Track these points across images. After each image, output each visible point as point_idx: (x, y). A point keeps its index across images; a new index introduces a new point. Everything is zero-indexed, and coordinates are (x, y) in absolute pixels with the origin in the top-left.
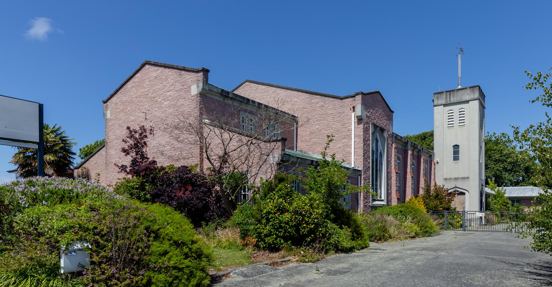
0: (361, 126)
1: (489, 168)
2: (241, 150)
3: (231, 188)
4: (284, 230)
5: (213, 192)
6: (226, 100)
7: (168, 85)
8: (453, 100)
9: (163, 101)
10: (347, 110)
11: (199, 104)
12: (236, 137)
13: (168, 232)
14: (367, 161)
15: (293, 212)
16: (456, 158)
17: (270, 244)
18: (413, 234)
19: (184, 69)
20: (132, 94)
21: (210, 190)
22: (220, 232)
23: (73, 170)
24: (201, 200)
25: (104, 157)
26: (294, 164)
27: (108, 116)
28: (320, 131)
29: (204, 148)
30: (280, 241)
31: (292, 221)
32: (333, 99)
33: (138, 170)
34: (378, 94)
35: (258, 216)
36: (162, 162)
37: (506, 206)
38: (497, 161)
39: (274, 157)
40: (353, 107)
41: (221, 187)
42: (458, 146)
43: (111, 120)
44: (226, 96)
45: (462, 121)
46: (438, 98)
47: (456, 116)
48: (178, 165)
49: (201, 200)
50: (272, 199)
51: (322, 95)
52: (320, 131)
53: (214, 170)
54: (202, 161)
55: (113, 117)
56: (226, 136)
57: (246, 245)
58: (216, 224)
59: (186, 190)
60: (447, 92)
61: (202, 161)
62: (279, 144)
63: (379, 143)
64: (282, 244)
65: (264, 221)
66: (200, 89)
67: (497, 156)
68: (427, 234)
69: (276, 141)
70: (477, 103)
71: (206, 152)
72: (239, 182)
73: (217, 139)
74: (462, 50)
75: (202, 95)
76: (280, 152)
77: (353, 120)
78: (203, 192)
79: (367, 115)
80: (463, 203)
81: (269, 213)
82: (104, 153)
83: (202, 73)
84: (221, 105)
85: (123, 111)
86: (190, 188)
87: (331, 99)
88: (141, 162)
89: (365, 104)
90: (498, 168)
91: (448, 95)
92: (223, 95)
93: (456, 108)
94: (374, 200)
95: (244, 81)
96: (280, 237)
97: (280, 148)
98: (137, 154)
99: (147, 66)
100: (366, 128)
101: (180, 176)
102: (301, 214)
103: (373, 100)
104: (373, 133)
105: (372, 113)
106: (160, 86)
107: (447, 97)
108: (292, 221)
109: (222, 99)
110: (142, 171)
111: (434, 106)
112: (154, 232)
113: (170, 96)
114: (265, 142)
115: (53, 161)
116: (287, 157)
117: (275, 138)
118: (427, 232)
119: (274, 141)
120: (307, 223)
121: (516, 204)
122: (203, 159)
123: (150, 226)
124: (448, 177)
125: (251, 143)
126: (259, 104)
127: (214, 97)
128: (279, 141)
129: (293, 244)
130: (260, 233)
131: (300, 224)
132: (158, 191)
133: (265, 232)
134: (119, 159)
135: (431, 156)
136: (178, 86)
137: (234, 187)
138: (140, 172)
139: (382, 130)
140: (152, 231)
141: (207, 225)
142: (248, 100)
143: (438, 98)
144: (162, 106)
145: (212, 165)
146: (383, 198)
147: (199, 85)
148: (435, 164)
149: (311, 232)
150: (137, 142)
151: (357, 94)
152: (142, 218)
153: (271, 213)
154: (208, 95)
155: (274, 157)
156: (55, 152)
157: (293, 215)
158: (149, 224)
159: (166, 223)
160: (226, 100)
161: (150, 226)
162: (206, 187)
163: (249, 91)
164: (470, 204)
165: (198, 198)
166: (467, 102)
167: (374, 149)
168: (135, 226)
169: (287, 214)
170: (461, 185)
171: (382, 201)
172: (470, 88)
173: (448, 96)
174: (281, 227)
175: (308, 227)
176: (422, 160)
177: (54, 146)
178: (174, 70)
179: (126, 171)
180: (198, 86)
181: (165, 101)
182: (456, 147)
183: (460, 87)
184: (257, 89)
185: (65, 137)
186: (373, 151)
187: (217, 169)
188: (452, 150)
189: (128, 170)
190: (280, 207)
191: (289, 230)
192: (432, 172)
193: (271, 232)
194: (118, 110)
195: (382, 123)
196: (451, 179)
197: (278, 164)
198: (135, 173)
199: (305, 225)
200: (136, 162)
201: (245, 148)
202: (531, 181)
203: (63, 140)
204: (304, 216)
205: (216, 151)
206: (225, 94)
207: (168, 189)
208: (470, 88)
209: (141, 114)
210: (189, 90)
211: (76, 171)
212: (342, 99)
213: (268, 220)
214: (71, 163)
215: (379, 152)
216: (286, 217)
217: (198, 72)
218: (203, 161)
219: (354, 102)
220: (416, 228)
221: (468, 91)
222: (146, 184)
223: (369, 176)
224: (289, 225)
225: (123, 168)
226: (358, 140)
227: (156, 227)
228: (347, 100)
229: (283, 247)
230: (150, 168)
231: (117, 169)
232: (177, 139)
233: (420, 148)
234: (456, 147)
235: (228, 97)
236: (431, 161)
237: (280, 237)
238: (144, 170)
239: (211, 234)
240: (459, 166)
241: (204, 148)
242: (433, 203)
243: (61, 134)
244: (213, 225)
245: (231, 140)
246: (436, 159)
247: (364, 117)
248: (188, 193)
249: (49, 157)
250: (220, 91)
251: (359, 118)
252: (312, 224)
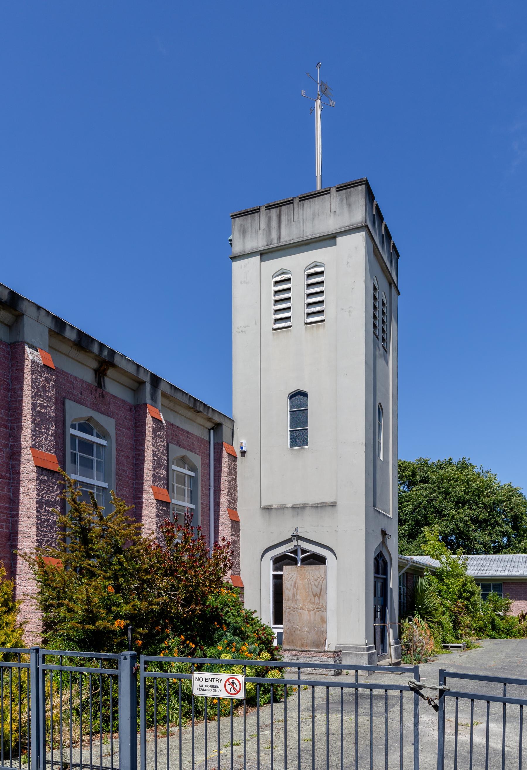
1: (445, 516)
8: (289, 234)
16: (299, 437)
37: (468, 599)
38: (460, 503)
42: (305, 395)
45: (316, 310)
67: (459, 491)
90: (462, 516)
93: (296, 264)
107: (269, 225)
111: (234, 258)
121: (491, 595)
148: (233, 458)
166: (330, 239)
172: (339, 189)
173: (274, 223)
182: (299, 397)
188: (283, 410)
192: (224, 484)
196: (281, 508)
221: (335, 200)
234: (299, 397)
236: (218, 447)
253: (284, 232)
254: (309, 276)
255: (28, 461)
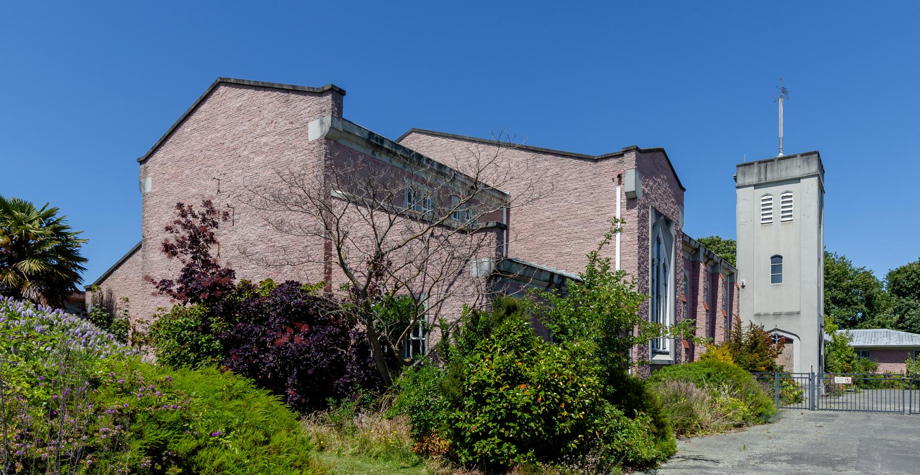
0: (635, 211)
2: (411, 250)
3: (391, 328)
4: (520, 424)
5: (351, 335)
6: (377, 155)
7: (263, 123)
8: (770, 177)
9: (251, 156)
10: (607, 181)
11: (323, 158)
12: (400, 224)
13: (222, 458)
14: (644, 278)
15: (538, 383)
17: (484, 457)
18: (739, 420)
19: (295, 90)
20: (193, 143)
21: (344, 331)
22: (365, 418)
23: (84, 293)
24: (328, 352)
25: (140, 267)
26: (523, 279)
27: (149, 188)
28: (553, 221)
29: (334, 241)
30: (509, 448)
31: (538, 405)
32: (578, 161)
33: (195, 289)
34: (661, 153)
35: (454, 390)
36: (248, 273)
39: (479, 265)
40: (619, 176)
41: (369, 326)
42: (781, 257)
43: (153, 194)
44: (377, 146)
45: (787, 214)
46: (744, 174)
47: (777, 205)
48: (279, 280)
49: (328, 352)
50: (487, 351)
51: (556, 154)
52: (553, 221)
53: (355, 289)
54: (328, 272)
55: (157, 189)
56: (382, 220)
57: (425, 453)
58: (357, 402)
59: (297, 331)
60: (760, 162)
61: (328, 272)
62: (492, 235)
63: (663, 246)
64: (513, 456)
65: (469, 402)
66: (326, 128)
68: (762, 420)
69: (485, 230)
70: (814, 181)
71: (339, 249)
72: (405, 316)
73: (360, 226)
74: (784, 91)
75: (331, 139)
76: (493, 253)
77: (619, 199)
78: (330, 335)
79: (644, 191)
80: (790, 358)
81: (481, 385)
82: (140, 259)
83: (329, 97)
84: (365, 161)
85: (175, 177)
86: (305, 328)
87: (574, 161)
88: (204, 274)
89: (642, 171)
91: (763, 168)
92: (371, 143)
94: (655, 353)
95: (408, 131)
96: (507, 440)
97: (494, 245)
98: (194, 258)
99: (222, 89)
100: (643, 215)
101: (282, 303)
102: (556, 389)
103: (654, 162)
104: (654, 227)
105: (651, 188)
106: (247, 126)
108: (538, 405)
109: (370, 151)
110: (202, 291)
111: (738, 187)
112: (178, 461)
113: (266, 144)
114: (462, 232)
115: (37, 273)
116: (507, 264)
117: (482, 225)
118: (760, 415)
119: (481, 230)
120: (570, 408)
122: (330, 269)
123: (166, 441)
124: (762, 311)
125: (432, 235)
126: (440, 166)
127: (354, 146)
128: (491, 229)
129: (539, 456)
130: (458, 431)
131: (555, 412)
132: (237, 332)
133: (474, 428)
134: (167, 271)
135: (732, 276)
136: (283, 124)
137: (397, 325)
138: (200, 294)
139: (668, 222)
140: (170, 457)
141: (338, 405)
142: (420, 157)
143: (744, 174)
144: (251, 164)
145: (351, 277)
146: (668, 349)
147: (324, 120)
149: (580, 427)
150: (196, 234)
151: (628, 151)
152: (140, 417)
153: (489, 385)
154: (343, 142)
155: (479, 265)
156: (44, 256)
157: (540, 391)
158: (164, 434)
159: (221, 430)
160: (377, 155)
161: (166, 441)
162: (336, 326)
163: (416, 143)
164: (801, 359)
165: (320, 348)
166: (797, 180)
167: (655, 257)
168: (117, 445)
169: (523, 386)
170: (784, 325)
171: (667, 353)
172: (802, 155)
173: (763, 171)
174: (511, 417)
175: (572, 418)
176: (720, 281)
177: (42, 243)
178: (275, 94)
179: (170, 291)
180: (322, 123)
181: (257, 155)
183: (781, 155)
184: (432, 145)
185: (64, 228)
186: (653, 261)
187: (362, 288)
189: (175, 288)
190: (508, 371)
191: (532, 424)
192: (735, 303)
193: (488, 429)
194: (167, 177)
195: (668, 208)
196: (766, 315)
197: (489, 279)
198: (188, 295)
199: (565, 413)
200: (191, 274)
201: (417, 246)
202: (876, 320)
203: (58, 232)
204: (562, 392)
205: (358, 255)
206: (375, 142)
207: (257, 330)
208: (802, 155)
209: (209, 183)
210: (303, 130)
211: (89, 295)
212: (596, 161)
213: (481, 401)
214: (76, 277)
215: (662, 262)
216: (522, 394)
217: (321, 93)
218: (330, 272)
219: (620, 166)
220: (743, 408)
221: (798, 161)
222: (211, 318)
223: (647, 307)
224: (530, 412)
225: (165, 286)
226: (628, 238)
227: (185, 445)
228: (606, 162)
229: (515, 464)
230: (220, 286)
231: (151, 288)
232: (279, 227)
233: (711, 264)
235: (382, 148)
237: (507, 440)
238: (209, 287)
239: (348, 424)
240: (779, 295)
241: (334, 241)
242: (749, 358)
243: (55, 223)
244: (352, 406)
245: (391, 225)
246: (741, 280)
247: (640, 195)
248: (299, 338)
249: (28, 266)
250: (366, 135)
251: (631, 196)
252: (580, 411)
253: (769, 175)
254: (783, 198)
255: (901, 339)
